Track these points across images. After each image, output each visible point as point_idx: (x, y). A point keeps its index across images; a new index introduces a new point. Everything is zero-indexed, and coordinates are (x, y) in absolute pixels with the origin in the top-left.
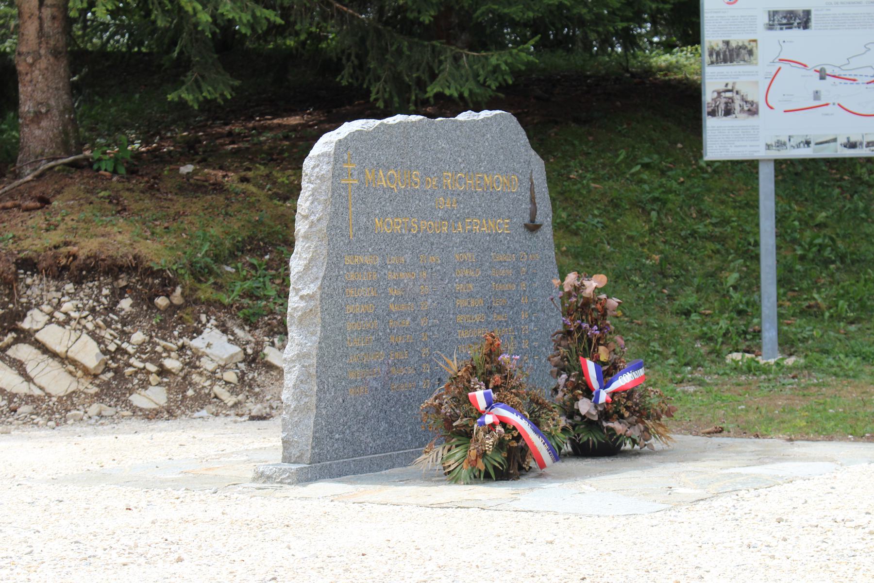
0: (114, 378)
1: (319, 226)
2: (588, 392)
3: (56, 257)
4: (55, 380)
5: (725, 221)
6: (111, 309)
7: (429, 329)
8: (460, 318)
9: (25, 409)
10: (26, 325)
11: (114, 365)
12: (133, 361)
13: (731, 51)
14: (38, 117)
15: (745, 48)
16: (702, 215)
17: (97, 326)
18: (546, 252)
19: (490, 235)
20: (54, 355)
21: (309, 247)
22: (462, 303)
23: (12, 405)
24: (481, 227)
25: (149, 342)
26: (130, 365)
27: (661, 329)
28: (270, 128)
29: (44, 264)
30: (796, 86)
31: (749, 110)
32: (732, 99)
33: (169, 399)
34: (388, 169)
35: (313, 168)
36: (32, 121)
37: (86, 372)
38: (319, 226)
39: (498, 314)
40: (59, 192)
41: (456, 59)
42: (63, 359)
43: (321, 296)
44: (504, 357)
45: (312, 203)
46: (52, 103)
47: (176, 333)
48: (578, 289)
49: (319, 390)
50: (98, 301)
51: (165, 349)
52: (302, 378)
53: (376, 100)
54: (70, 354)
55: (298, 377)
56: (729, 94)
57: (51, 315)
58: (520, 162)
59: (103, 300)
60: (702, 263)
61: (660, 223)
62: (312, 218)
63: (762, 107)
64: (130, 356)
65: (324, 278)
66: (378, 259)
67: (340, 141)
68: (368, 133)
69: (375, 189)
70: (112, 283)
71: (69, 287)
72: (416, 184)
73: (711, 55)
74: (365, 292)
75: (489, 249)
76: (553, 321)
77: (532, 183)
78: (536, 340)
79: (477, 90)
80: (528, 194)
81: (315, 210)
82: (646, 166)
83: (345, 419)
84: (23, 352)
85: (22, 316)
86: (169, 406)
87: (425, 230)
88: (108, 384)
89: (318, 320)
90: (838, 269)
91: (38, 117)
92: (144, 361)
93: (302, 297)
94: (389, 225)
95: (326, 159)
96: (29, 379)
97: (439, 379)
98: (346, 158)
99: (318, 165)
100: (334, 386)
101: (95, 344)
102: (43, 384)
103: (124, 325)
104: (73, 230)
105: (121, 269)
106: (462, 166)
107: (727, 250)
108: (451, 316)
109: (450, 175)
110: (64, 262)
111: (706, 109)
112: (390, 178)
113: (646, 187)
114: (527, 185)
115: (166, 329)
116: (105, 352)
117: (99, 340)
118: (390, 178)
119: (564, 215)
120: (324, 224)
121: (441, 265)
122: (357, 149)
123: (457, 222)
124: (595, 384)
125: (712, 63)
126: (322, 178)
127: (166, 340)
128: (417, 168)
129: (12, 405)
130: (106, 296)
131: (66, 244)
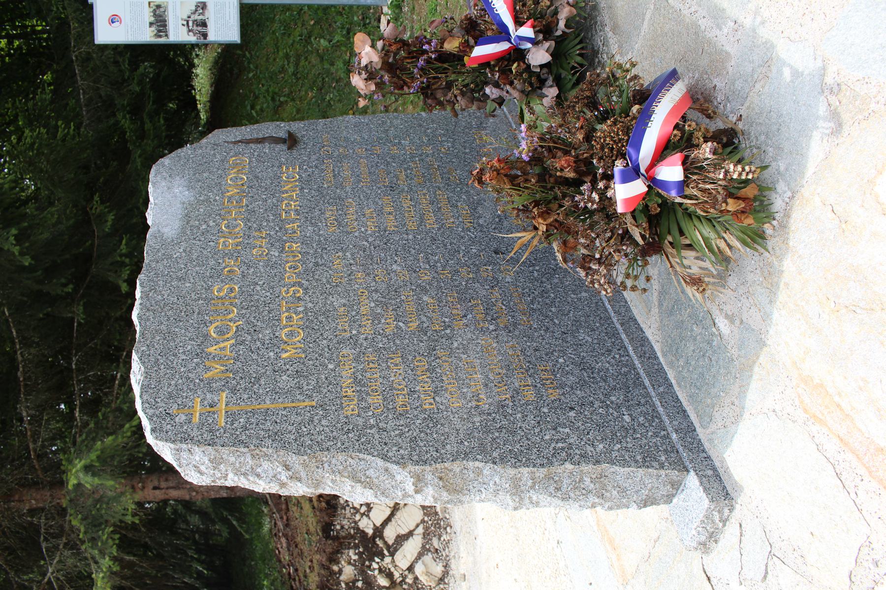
1: (298, 467)
2: (517, 54)
3: (321, 510)
5: (287, 56)
8: (412, 225)
9: (435, 542)
10: (370, 532)
16: (283, 70)
19: (302, 189)
20: (392, 515)
22: (391, 223)
24: (291, 200)
29: (326, 518)
31: (202, 9)
34: (207, 336)
35: (201, 473)
38: (298, 467)
39: (398, 179)
43: (417, 463)
44: (524, 150)
45: (258, 476)
48: (371, 75)
49: (569, 458)
52: (552, 489)
54: (392, 506)
56: (191, 24)
57: (363, 515)
58: (214, 154)
60: (314, 66)
61: (288, 96)
65: (385, 458)
66: (345, 352)
69: (236, 359)
72: (232, 290)
73: (160, 36)
74: (397, 375)
75: (319, 189)
76: (395, 122)
77: (239, 141)
80: (253, 146)
81: (271, 474)
82: (252, 108)
83: (597, 404)
84: (390, 534)
87: (298, 275)
89: (456, 467)
94: (291, 334)
95: (185, 455)
96: (410, 534)
97: (496, 253)
98: (184, 417)
100: (555, 429)
106: (211, 223)
108: (411, 237)
109: (222, 240)
110: (324, 504)
113: (265, 105)
118: (221, 332)
120: (294, 460)
122: (170, 396)
123: (286, 230)
124: (504, 46)
125: (166, 35)
126: (216, 463)
128: (209, 289)
129: (432, 550)
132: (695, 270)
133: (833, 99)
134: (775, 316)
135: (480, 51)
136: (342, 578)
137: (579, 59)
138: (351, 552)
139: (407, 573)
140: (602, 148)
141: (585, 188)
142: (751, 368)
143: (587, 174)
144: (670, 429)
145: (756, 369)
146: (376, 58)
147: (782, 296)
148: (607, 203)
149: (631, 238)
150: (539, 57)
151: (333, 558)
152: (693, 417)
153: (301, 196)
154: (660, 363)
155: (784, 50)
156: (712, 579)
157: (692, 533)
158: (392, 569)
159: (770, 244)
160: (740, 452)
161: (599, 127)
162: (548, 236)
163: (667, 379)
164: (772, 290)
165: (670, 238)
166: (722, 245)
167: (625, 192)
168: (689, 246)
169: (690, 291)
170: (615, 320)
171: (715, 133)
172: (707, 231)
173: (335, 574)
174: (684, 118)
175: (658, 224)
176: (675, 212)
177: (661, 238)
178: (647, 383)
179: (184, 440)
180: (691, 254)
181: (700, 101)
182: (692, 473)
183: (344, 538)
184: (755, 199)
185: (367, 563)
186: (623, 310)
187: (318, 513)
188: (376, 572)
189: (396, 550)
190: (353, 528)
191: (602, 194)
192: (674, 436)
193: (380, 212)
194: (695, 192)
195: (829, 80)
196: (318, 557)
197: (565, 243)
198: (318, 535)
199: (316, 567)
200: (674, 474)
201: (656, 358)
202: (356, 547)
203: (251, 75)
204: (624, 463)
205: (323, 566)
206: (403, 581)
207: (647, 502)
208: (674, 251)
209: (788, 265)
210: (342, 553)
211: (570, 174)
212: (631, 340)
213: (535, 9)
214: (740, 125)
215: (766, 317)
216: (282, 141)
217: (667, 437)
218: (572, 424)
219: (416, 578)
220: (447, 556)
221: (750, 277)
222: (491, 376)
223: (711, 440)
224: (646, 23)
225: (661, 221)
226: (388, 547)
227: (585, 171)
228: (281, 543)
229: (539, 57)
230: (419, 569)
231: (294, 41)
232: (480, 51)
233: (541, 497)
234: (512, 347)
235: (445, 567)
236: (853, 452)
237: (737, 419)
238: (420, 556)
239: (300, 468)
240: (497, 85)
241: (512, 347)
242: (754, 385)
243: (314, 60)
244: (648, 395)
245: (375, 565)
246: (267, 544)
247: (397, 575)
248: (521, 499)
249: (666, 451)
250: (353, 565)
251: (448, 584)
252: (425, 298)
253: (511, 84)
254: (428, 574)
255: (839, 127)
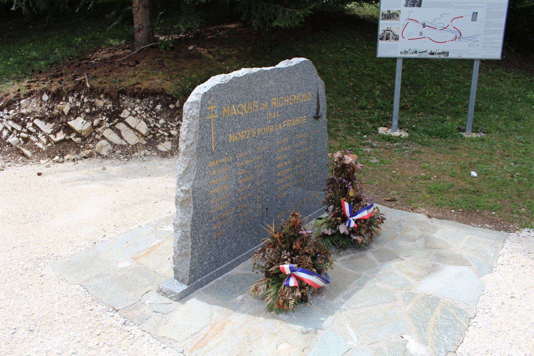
0: (152, 138)
1: (192, 148)
2: (345, 219)
3: (133, 89)
4: (131, 138)
5: (373, 69)
6: (153, 109)
7: (262, 185)
8: (279, 174)
9: (118, 151)
11: (153, 132)
12: (159, 131)
13: (390, 14)
14: (140, 30)
15: (396, 13)
17: (147, 117)
18: (323, 127)
19: (296, 126)
20: (131, 128)
21: (186, 160)
22: (279, 166)
23: (114, 150)
25: (166, 123)
26: (159, 133)
27: (354, 116)
28: (224, 29)
29: (128, 92)
30: (414, 29)
32: (389, 34)
33: (172, 148)
34: (238, 103)
35: (189, 110)
36: (138, 31)
37: (142, 135)
38: (192, 148)
40: (143, 58)
41: (284, 12)
42: (134, 130)
43: (193, 191)
45: (188, 132)
46: (144, 25)
47: (176, 119)
50: (148, 106)
51: (172, 127)
52: (182, 238)
53: (254, 26)
54: (136, 128)
55: (180, 237)
56: (388, 32)
57: (131, 112)
59: (150, 106)
62: (187, 142)
63: (400, 37)
64: (159, 129)
65: (195, 179)
67: (205, 93)
68: (225, 84)
70: (154, 99)
71: (138, 101)
72: (255, 108)
73: (382, 16)
75: (295, 133)
77: (318, 95)
78: (316, 171)
79: (291, 24)
82: (347, 48)
83: (211, 252)
84: (121, 126)
85: (121, 112)
86: (172, 150)
87: (260, 133)
88: (150, 140)
89: (191, 205)
90: (410, 88)
91: (140, 30)
92: (163, 131)
93: (182, 190)
95: (196, 105)
96: (122, 138)
97: (267, 209)
99: (191, 109)
101: (145, 124)
102: (127, 140)
103: (157, 116)
104: (142, 77)
105: (157, 94)
107: (374, 80)
110: (136, 91)
111: (379, 37)
112: (239, 109)
114: (316, 96)
115: (172, 117)
116: (149, 127)
117: (147, 122)
119: (320, 67)
120: (194, 147)
121: (269, 150)
124: (348, 214)
125: (383, 19)
126: (193, 117)
127: (172, 123)
128: (256, 99)
129: (114, 150)
130: (151, 104)
131: (138, 84)
132: (260, 287)
133: (313, 332)
134: (244, 315)
135: (346, 205)
136: (97, 99)
137: (341, 243)
138: (111, 105)
139: (101, 135)
140: (302, 259)
141: (289, 253)
142: (226, 307)
143: (294, 253)
144: (202, 278)
145: (226, 309)
146: (347, 162)
147: (251, 317)
148: (283, 261)
149: (272, 267)
150: (342, 229)
151: (107, 96)
152: (206, 286)
153: (293, 127)
154: (224, 274)
155: (331, 318)
156: (147, 294)
157: (165, 287)
158: (102, 127)
159: (268, 313)
160: (194, 304)
161: (310, 257)
162: (273, 238)
163: (218, 277)
164: (253, 314)
165: (271, 280)
166: (268, 298)
167: (286, 267)
168: (268, 287)
169: (253, 287)
170: (240, 256)
171: (305, 296)
172: (273, 293)
173: (99, 96)
174: (310, 286)
175: (276, 276)
176: (280, 282)
177: (271, 277)
178: (218, 269)
179: (202, 106)
180: (265, 286)
181: (319, 291)
182: (188, 287)
183: (118, 102)
184: (283, 309)
185: (105, 114)
186: (243, 259)
187: (131, 88)
188: (101, 119)
189: (113, 129)
190: (124, 107)
191: (286, 260)
192: (199, 280)
193: (285, 160)
194: (286, 290)
195: (319, 331)
196: (108, 87)
197: (270, 244)
198: (120, 87)
199: (102, 86)
200: (187, 281)
201: (226, 272)
202: (114, 108)
203: (365, 47)
204: (191, 263)
205: (103, 90)
206: (96, 133)
207: (176, 271)
208: (266, 281)
209: (261, 319)
210: (110, 100)
211: (294, 247)
212: (232, 263)
213: (361, 228)
214: (308, 304)
215: (244, 312)
216: (317, 113)
217: (199, 278)
218: (204, 244)
219: (98, 140)
220: (112, 158)
221: (257, 307)
222: (221, 213)
223: (198, 293)
224: (351, 271)
225: (277, 278)
226: (114, 125)
227: (295, 252)
228: (106, 54)
229: (342, 229)
230: (104, 142)
231: (381, 74)
232: (346, 205)
233: (179, 234)
234: (231, 219)
235: (106, 156)
236: (204, 338)
237: (208, 303)
238: (111, 143)
239: (191, 149)
240: (334, 210)
241: (231, 219)
242: (221, 308)
243: (370, 86)
244: (213, 270)
245: (104, 118)
246: (103, 43)
247: (100, 129)
248: (178, 227)
249: (195, 277)
250: (104, 105)
251: (97, 158)
252: (250, 184)
253: (333, 217)
254: (102, 147)
255: (303, 333)
